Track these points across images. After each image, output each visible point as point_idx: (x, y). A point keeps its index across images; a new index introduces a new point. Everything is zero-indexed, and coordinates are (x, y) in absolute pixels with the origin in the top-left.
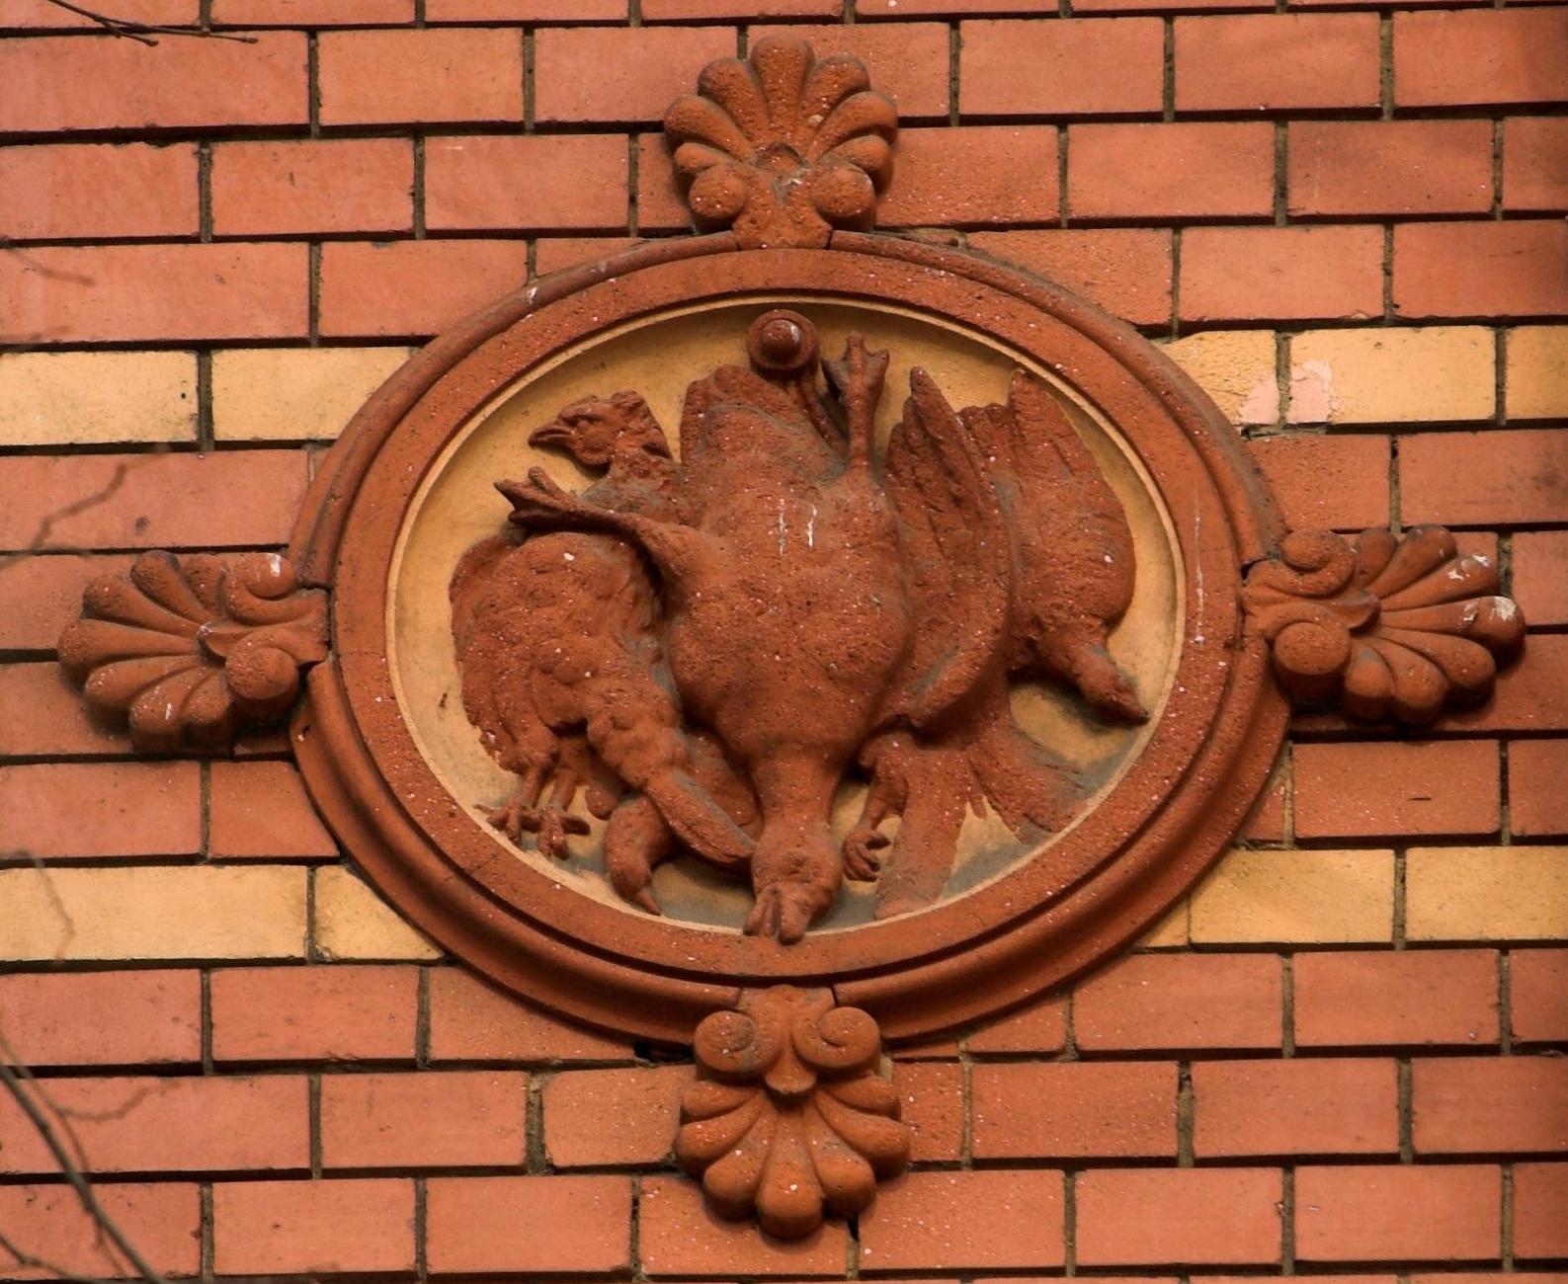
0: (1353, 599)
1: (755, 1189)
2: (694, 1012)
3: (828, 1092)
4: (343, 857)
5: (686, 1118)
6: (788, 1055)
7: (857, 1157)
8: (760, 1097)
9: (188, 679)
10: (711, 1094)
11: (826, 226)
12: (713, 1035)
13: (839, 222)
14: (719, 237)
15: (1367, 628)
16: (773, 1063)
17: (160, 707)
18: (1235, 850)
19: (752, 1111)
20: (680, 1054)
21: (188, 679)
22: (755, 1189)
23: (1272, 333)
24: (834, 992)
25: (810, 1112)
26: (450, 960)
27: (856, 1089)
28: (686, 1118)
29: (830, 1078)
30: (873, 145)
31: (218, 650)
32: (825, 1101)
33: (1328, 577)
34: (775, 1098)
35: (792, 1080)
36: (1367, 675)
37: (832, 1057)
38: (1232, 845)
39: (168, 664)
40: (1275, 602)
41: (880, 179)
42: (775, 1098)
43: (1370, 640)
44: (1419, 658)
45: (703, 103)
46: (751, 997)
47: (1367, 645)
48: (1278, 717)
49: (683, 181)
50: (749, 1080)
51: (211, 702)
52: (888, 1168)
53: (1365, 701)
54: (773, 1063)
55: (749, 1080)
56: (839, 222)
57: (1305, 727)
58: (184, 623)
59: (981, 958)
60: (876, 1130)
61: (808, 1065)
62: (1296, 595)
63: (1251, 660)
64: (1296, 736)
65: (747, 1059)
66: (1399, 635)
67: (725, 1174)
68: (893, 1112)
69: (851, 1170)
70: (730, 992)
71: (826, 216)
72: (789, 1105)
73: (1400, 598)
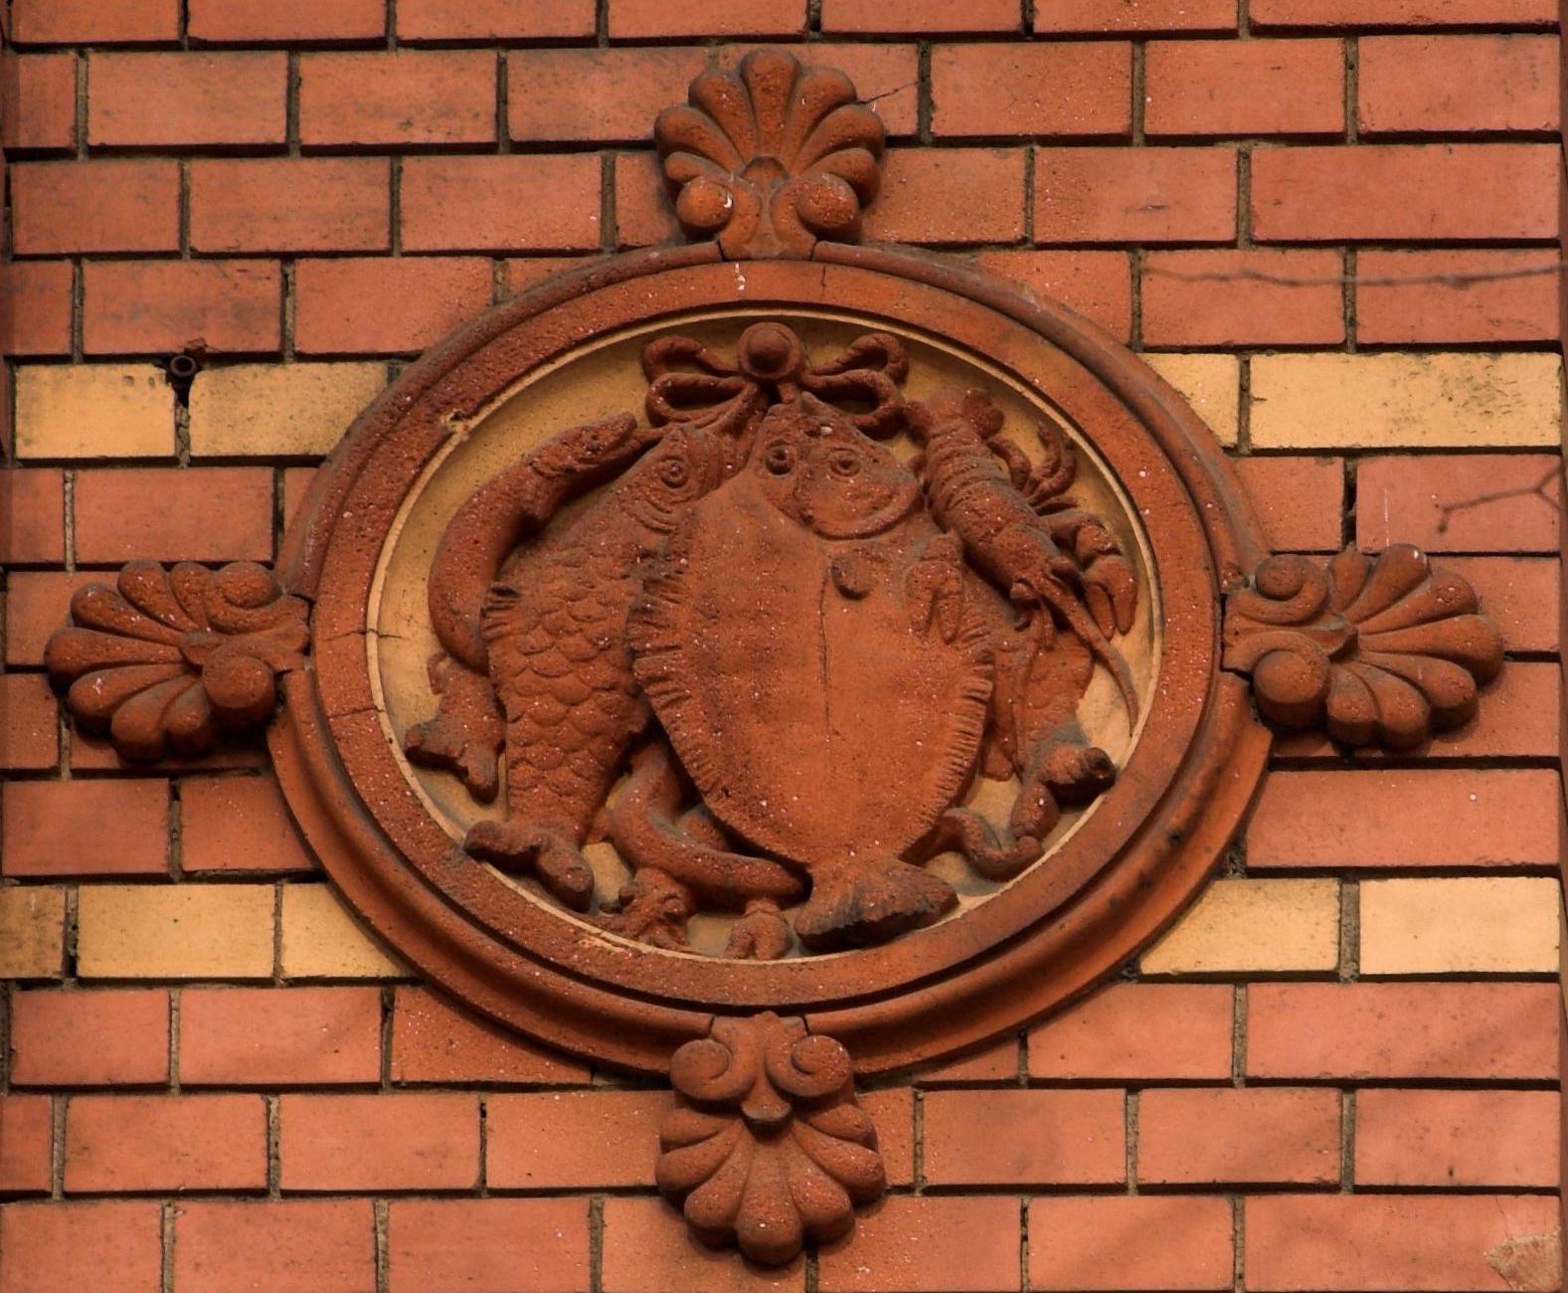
0: (1330, 624)
1: (734, 1214)
2: (670, 1039)
3: (805, 1121)
4: (314, 875)
5: (667, 1146)
6: (763, 1086)
7: (834, 1186)
8: (739, 1124)
9: (171, 688)
10: (690, 1121)
11: (812, 238)
12: (693, 1063)
13: (822, 233)
14: (708, 247)
15: (1347, 652)
16: (744, 1094)
17: (139, 717)
18: (740, 1237)
19: (733, 1132)
20: (659, 1082)
21: (171, 688)
22: (734, 1214)
23: (1232, 357)
24: (805, 1021)
25: (788, 1143)
26: (418, 979)
27: (828, 1117)
28: (667, 1146)
29: (805, 1107)
30: (860, 156)
31: (196, 660)
32: (798, 1126)
33: (1298, 607)
34: (749, 1123)
35: (766, 1107)
36: (1348, 702)
37: (807, 1086)
38: (1218, 872)
39: (149, 673)
40: (1249, 631)
41: (865, 192)
42: (749, 1123)
43: (1353, 665)
44: (1406, 685)
45: (696, 116)
46: (723, 1025)
47: (1349, 671)
48: (1258, 744)
49: (673, 189)
50: (727, 1108)
51: (189, 714)
52: (867, 1195)
53: (1352, 727)
54: (744, 1094)
55: (727, 1108)
56: (822, 233)
57: (1294, 751)
58: (166, 632)
59: (934, 997)
60: (852, 1156)
61: (782, 1093)
62: (1270, 623)
63: (1230, 689)
64: (1273, 764)
65: (718, 1089)
66: (1379, 658)
67: (707, 1201)
68: (869, 1141)
69: (829, 1198)
70: (701, 1019)
71: (809, 225)
72: (766, 1133)
73: (1373, 623)
